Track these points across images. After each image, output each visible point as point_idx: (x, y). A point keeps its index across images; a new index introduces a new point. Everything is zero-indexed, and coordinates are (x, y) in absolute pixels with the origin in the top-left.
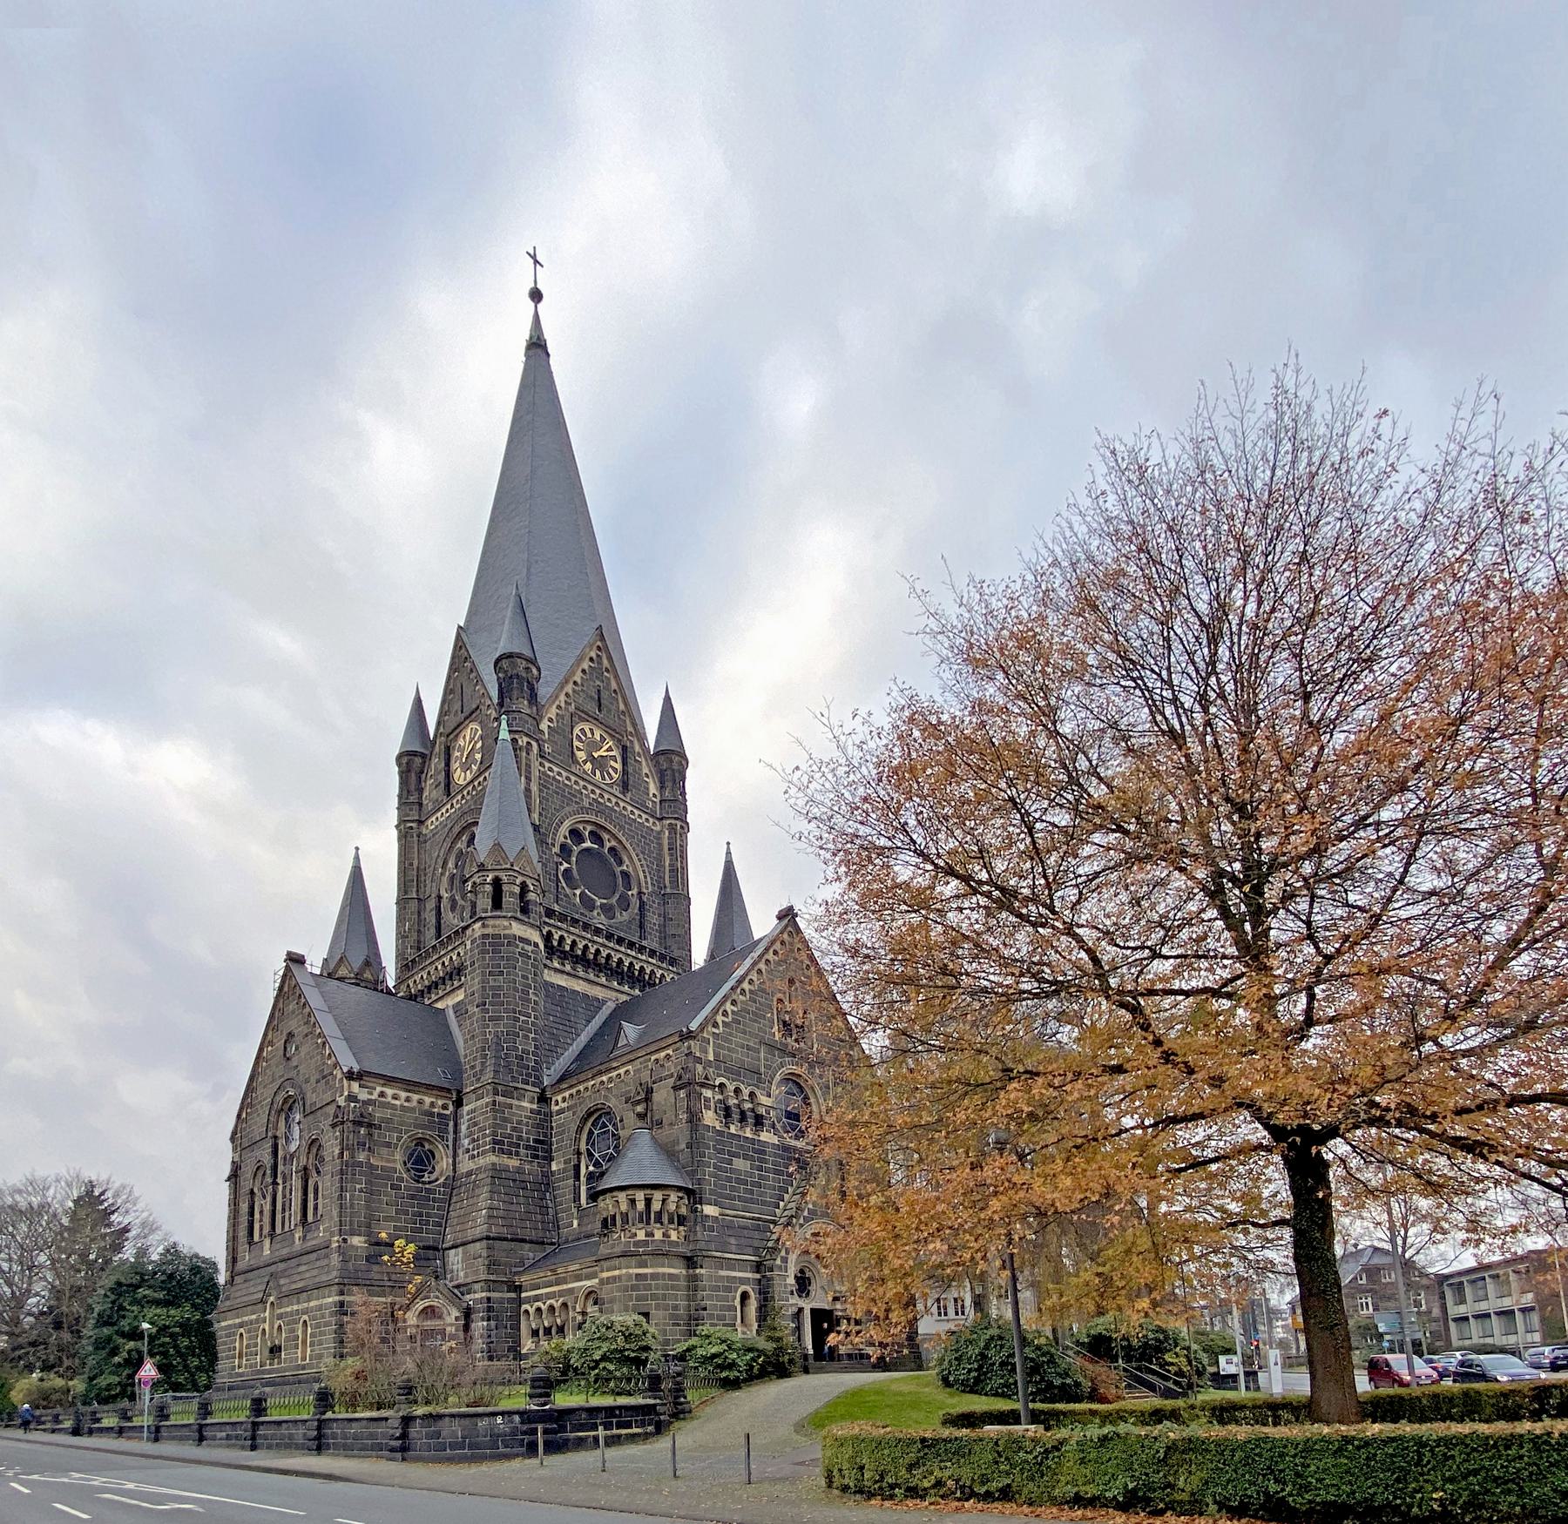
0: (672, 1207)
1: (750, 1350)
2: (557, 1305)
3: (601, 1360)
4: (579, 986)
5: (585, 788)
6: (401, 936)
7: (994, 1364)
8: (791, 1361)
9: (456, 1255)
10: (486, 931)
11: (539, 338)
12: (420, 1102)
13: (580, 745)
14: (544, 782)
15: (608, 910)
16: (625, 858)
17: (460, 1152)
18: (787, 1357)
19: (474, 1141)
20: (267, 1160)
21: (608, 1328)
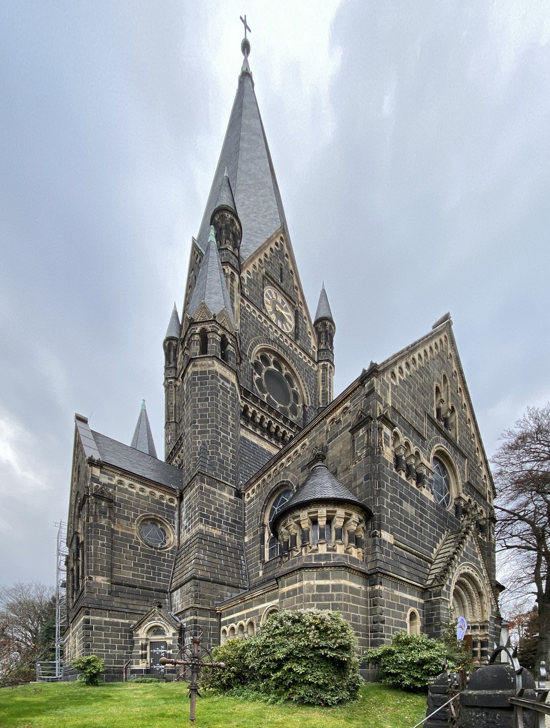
2: (245, 624)
3: (286, 659)
9: (177, 595)
10: (195, 369)
11: (247, 69)
13: (269, 301)
16: (295, 383)
17: (182, 530)
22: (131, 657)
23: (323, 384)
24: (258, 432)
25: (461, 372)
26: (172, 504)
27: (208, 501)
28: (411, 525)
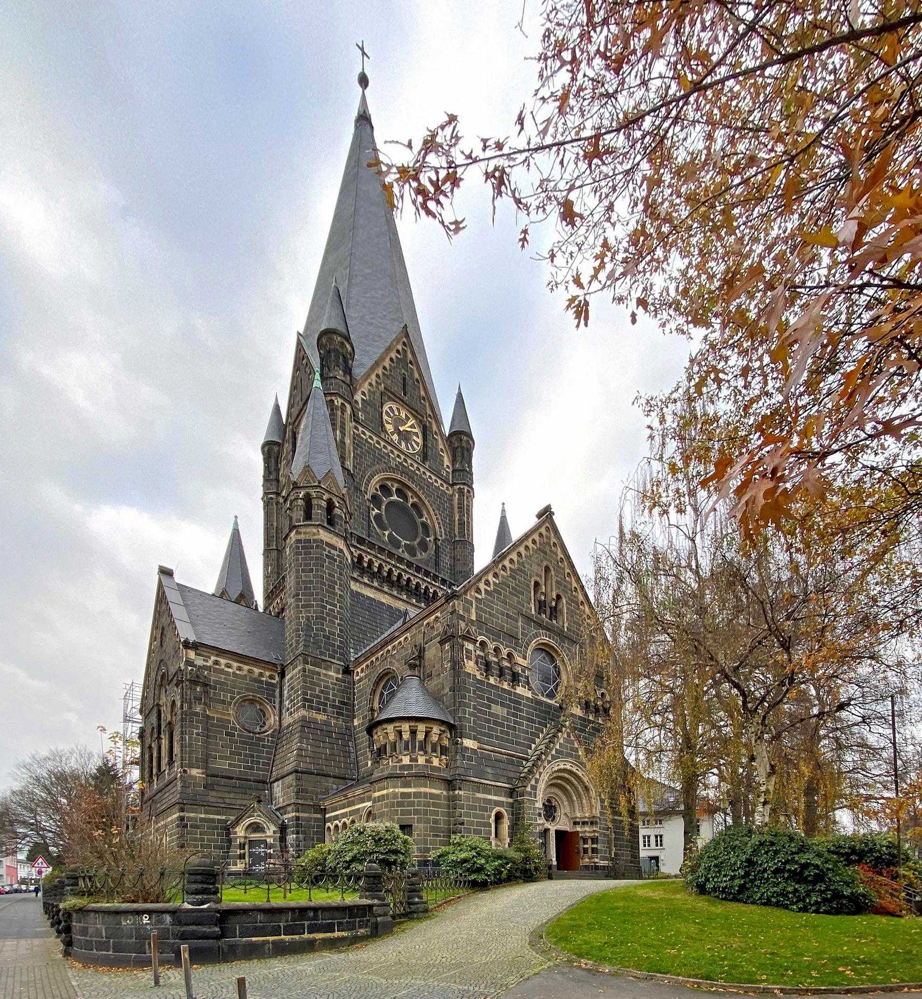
0: (435, 738)
1: (499, 857)
4: (385, 599)
5: (392, 452)
6: (267, 577)
7: (765, 870)
8: (536, 869)
9: (278, 786)
10: (299, 537)
11: (364, 112)
12: (250, 671)
13: (389, 420)
14: (358, 442)
15: (411, 550)
16: (425, 513)
17: (284, 711)
18: (533, 865)
19: (292, 701)
20: (155, 725)
21: (361, 833)
22: (228, 857)
23: (459, 512)
24: (376, 584)
25: (568, 557)
26: (273, 681)
27: (312, 683)
28: (502, 725)
